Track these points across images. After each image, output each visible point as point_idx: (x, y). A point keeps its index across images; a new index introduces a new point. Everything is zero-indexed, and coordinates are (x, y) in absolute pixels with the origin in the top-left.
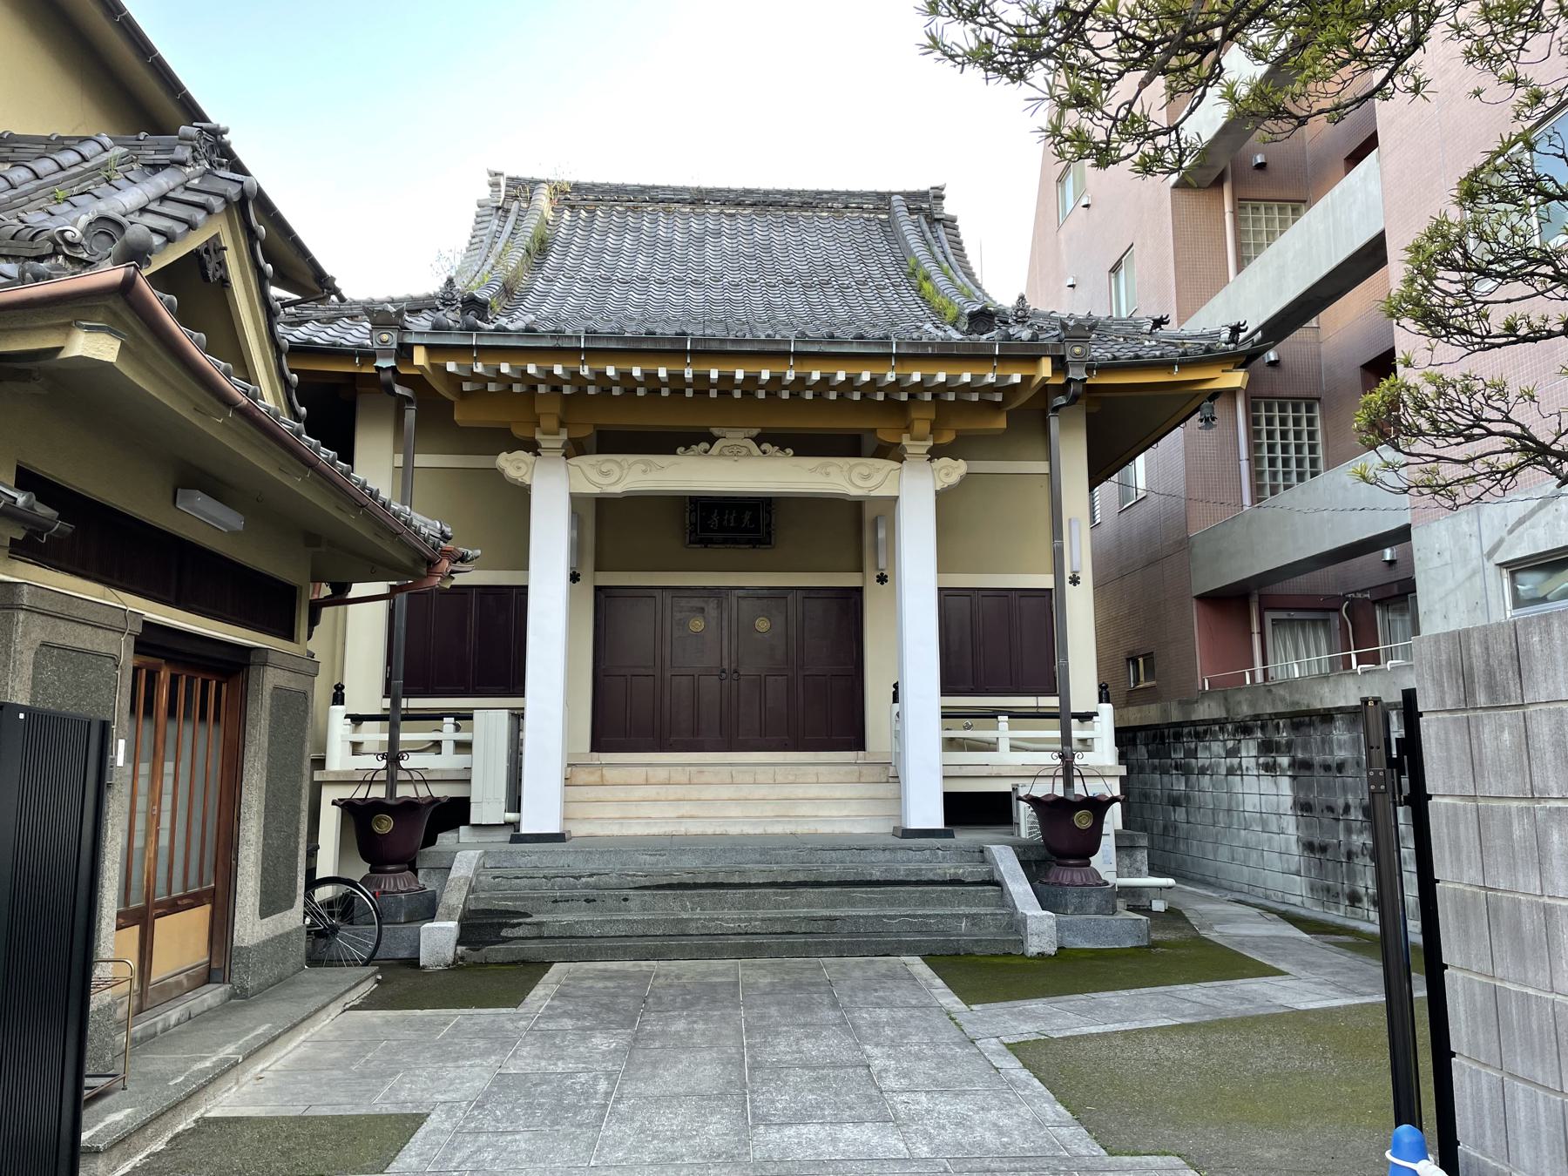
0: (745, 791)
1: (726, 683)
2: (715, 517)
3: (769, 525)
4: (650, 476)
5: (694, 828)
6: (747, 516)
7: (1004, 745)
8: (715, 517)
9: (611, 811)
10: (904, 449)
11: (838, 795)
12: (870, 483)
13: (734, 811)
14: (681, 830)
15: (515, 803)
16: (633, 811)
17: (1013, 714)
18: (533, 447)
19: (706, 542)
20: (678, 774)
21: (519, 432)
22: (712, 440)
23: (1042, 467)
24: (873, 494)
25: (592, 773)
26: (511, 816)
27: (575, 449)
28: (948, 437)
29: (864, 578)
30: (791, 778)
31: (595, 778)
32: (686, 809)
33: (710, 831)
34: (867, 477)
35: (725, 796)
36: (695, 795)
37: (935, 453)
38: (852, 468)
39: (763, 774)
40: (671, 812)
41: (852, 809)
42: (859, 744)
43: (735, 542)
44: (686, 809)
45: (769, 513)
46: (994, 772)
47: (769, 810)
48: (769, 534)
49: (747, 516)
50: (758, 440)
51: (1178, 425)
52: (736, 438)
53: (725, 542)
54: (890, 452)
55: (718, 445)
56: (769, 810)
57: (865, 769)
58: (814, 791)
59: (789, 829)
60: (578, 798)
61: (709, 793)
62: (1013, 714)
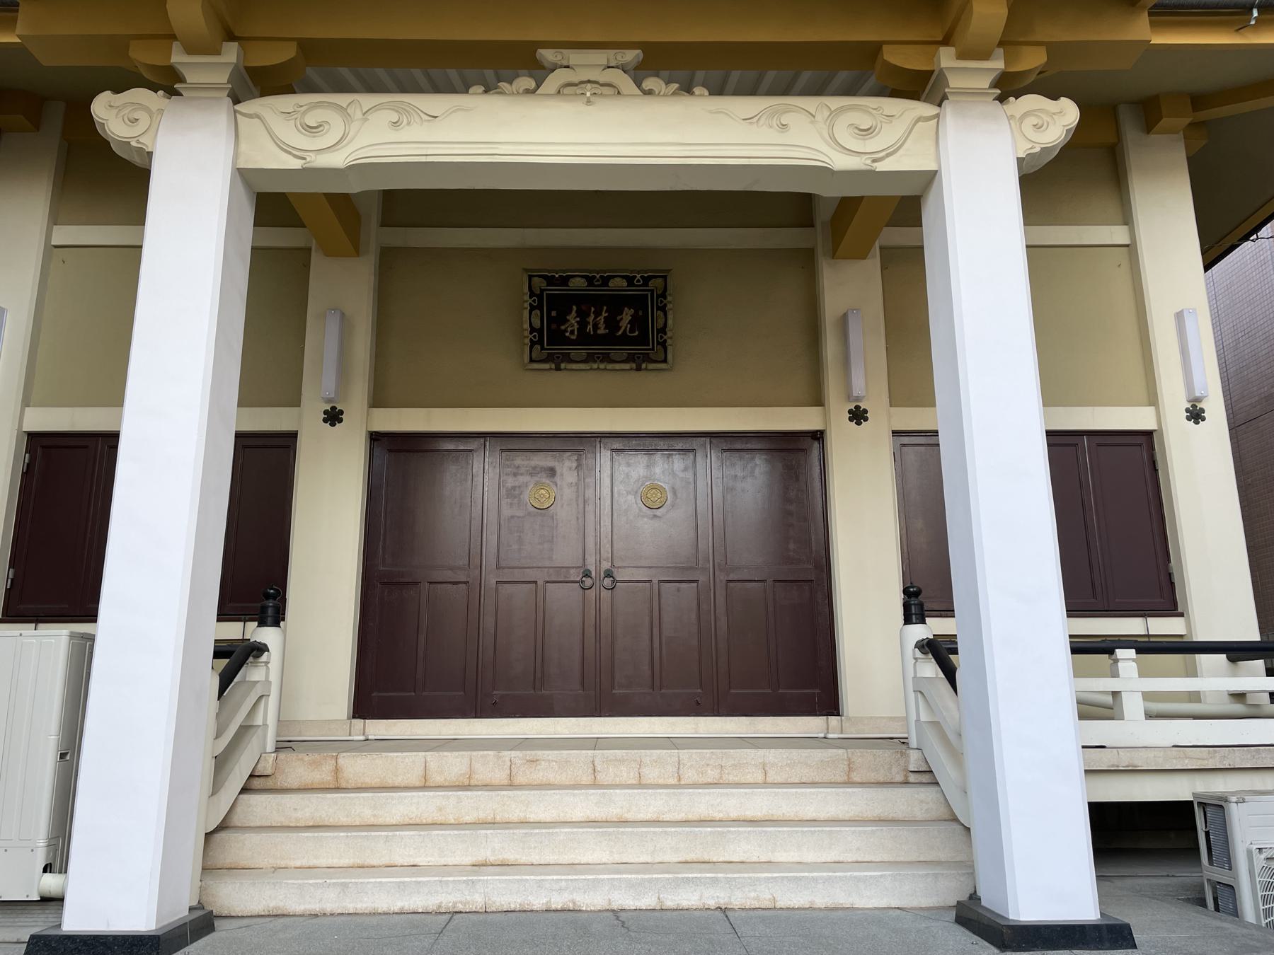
0: (619, 804)
1: (591, 594)
2: (573, 319)
3: (663, 330)
4: (407, 134)
5: (503, 894)
6: (626, 316)
7: (1133, 706)
8: (573, 319)
9: (334, 850)
10: (942, 75)
11: (810, 812)
12: (873, 145)
13: (595, 850)
14: (475, 900)
15: (56, 863)
16: (381, 850)
17: (1146, 646)
18: (168, 83)
19: (557, 361)
20: (489, 767)
21: (142, 56)
22: (539, 71)
23: (1118, 234)
24: (881, 167)
25: (315, 764)
26: (51, 883)
27: (260, 82)
28: (1032, 60)
29: (826, 418)
30: (712, 775)
31: (322, 775)
32: (494, 846)
33: (538, 902)
34: (867, 132)
35: (578, 815)
36: (516, 814)
37: (1008, 87)
38: (835, 114)
39: (657, 766)
40: (461, 851)
41: (850, 845)
42: (825, 700)
43: (606, 358)
44: (494, 846)
45: (663, 309)
46: (1124, 760)
47: (670, 847)
48: (663, 344)
49: (626, 316)
50: (638, 73)
51: (1246, 238)
52: (589, 64)
53: (590, 359)
54: (918, 86)
55: (554, 81)
56: (670, 847)
57: (862, 757)
58: (760, 804)
59: (712, 897)
60: (277, 819)
61: (542, 807)
62: (1146, 646)
